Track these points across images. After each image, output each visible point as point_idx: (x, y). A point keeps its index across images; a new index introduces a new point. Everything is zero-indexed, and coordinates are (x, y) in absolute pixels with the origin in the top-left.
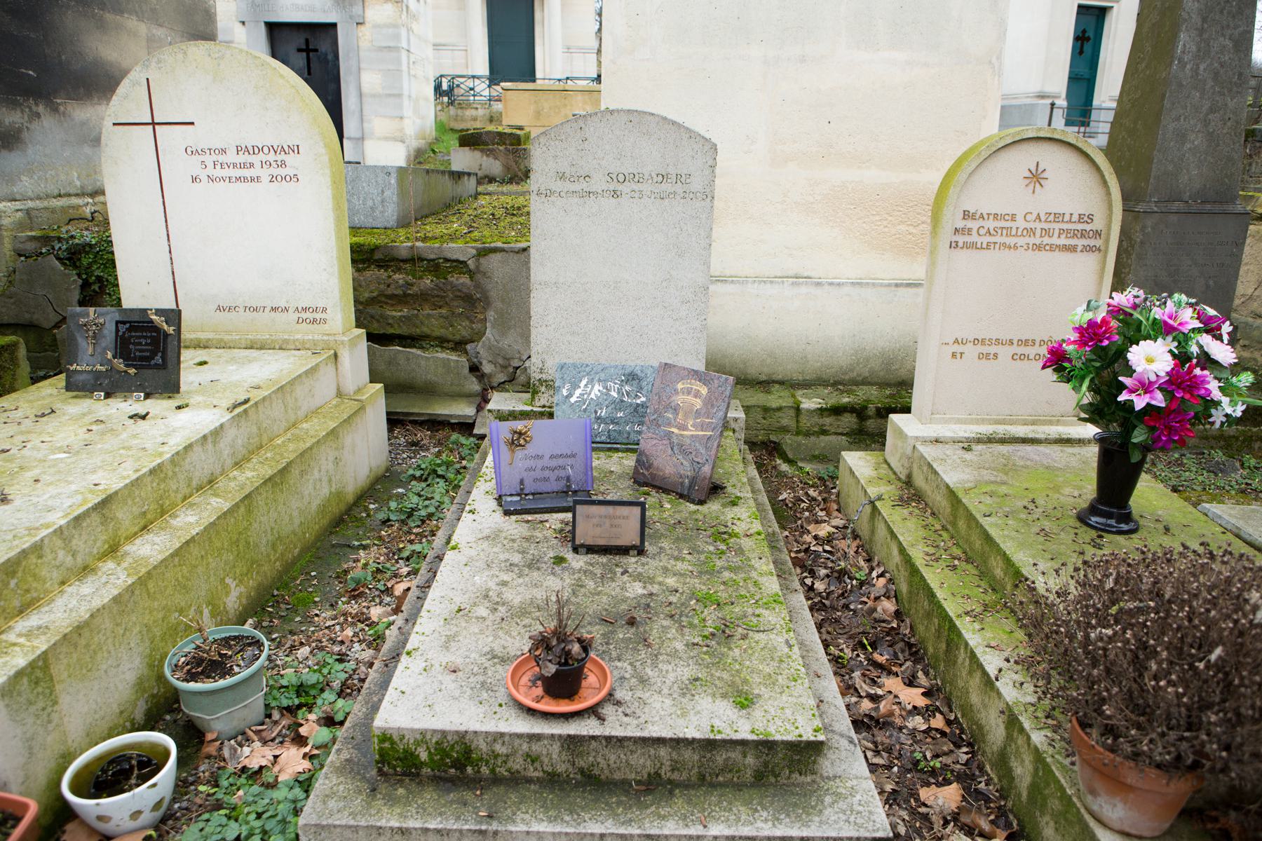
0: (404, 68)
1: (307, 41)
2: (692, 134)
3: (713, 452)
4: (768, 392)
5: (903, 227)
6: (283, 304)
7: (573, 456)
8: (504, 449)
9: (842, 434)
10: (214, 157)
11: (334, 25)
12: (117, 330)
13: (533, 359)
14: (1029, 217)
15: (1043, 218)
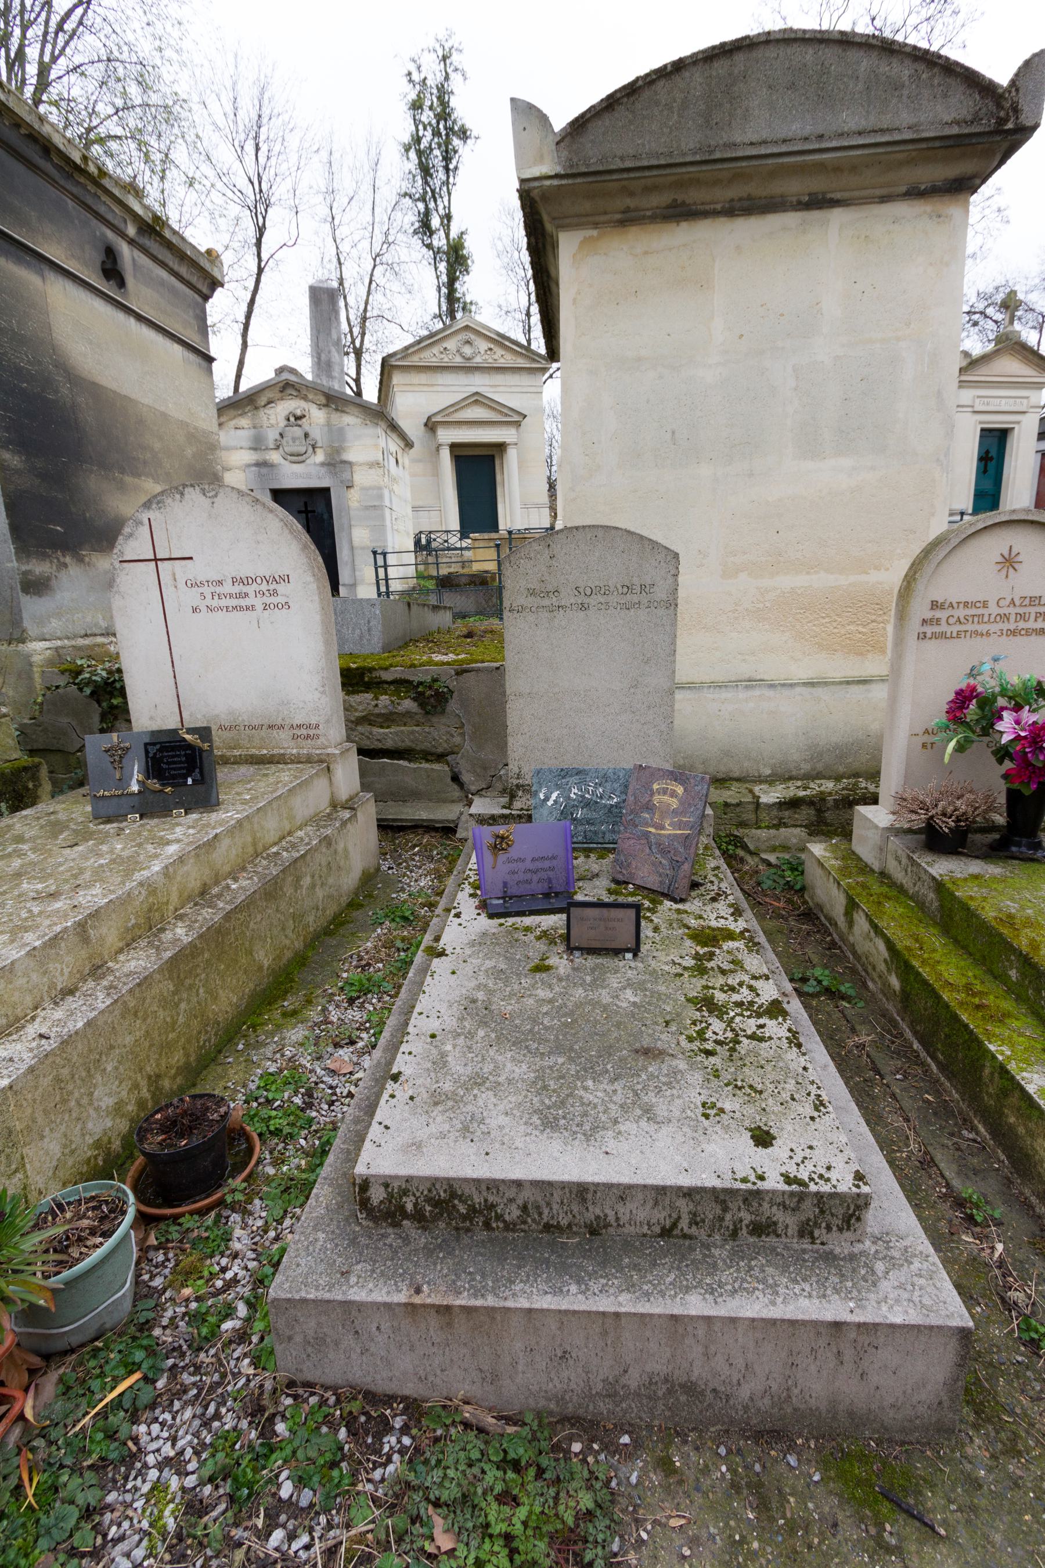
0: (388, 523)
1: (306, 504)
2: (654, 544)
3: (693, 850)
4: (728, 788)
5: (852, 627)
6: (279, 722)
7: (554, 858)
8: (488, 856)
9: (801, 826)
10: (212, 589)
11: (326, 491)
12: (147, 752)
13: (511, 766)
14: (1001, 603)
15: (1017, 603)
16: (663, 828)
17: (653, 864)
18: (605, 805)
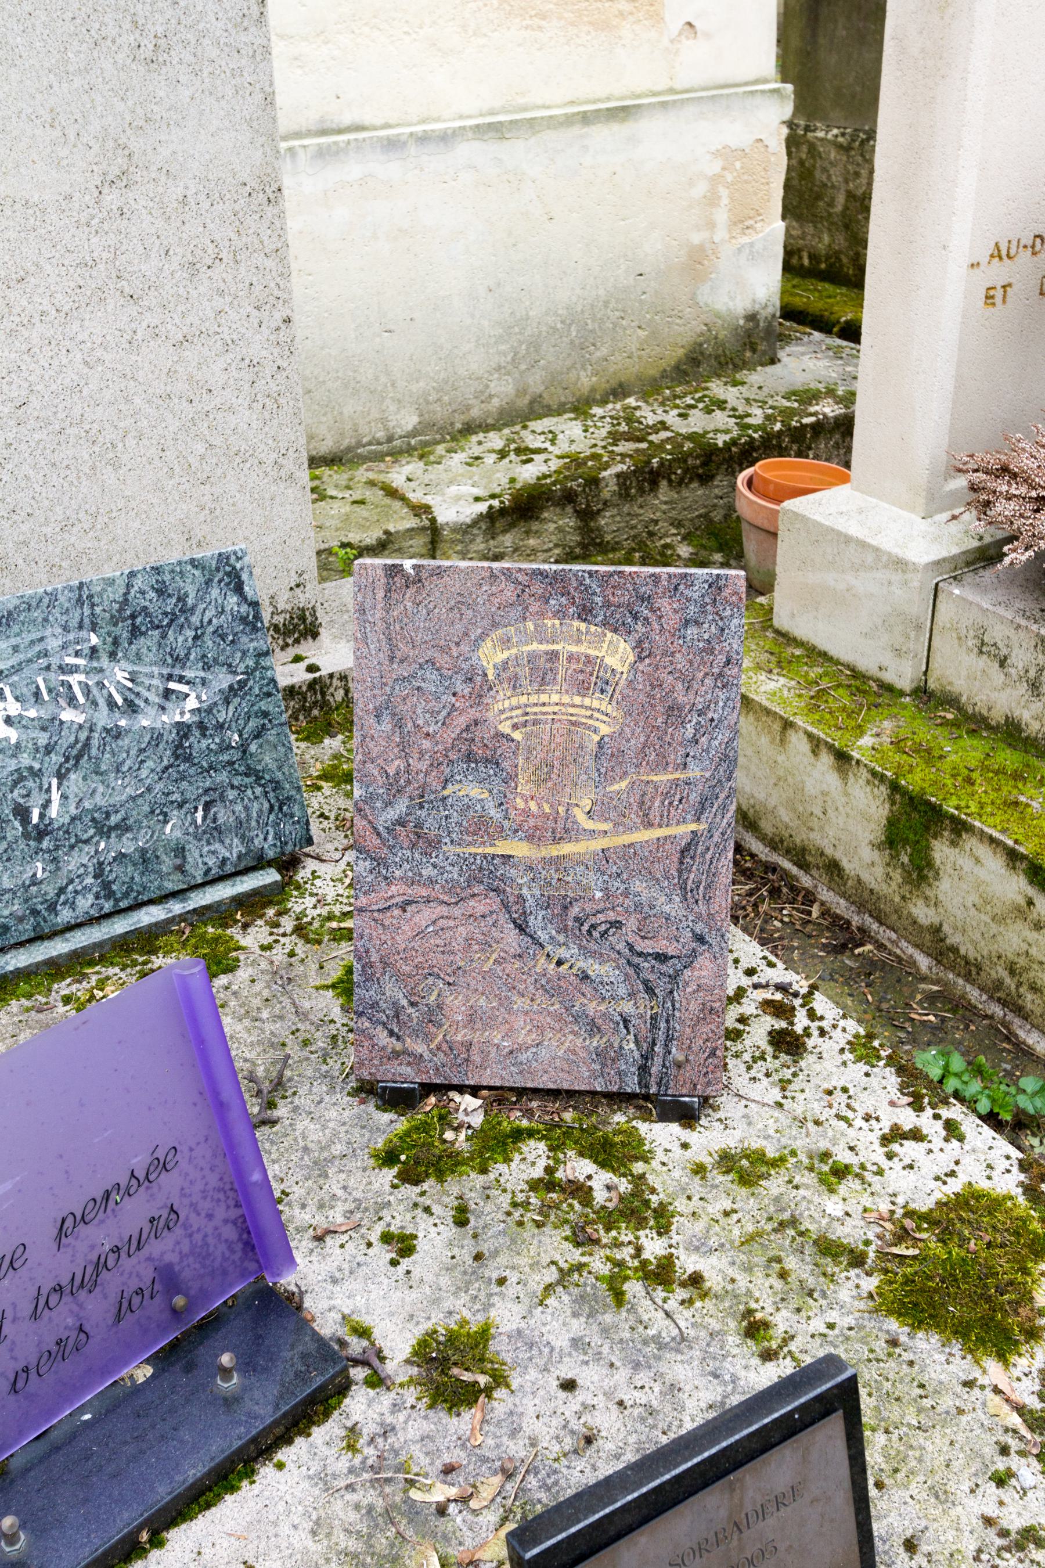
16: (567, 832)
17: (552, 989)
18: (157, 738)
